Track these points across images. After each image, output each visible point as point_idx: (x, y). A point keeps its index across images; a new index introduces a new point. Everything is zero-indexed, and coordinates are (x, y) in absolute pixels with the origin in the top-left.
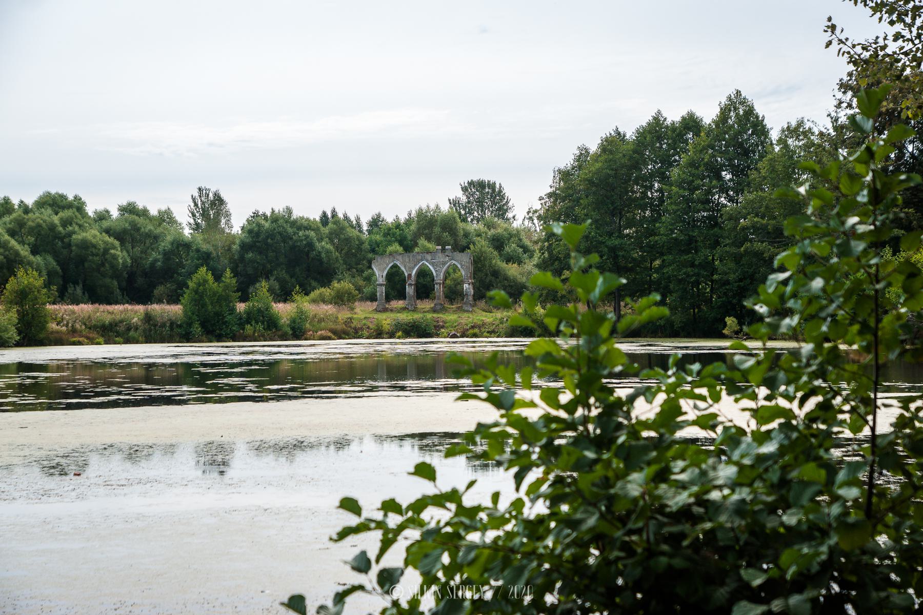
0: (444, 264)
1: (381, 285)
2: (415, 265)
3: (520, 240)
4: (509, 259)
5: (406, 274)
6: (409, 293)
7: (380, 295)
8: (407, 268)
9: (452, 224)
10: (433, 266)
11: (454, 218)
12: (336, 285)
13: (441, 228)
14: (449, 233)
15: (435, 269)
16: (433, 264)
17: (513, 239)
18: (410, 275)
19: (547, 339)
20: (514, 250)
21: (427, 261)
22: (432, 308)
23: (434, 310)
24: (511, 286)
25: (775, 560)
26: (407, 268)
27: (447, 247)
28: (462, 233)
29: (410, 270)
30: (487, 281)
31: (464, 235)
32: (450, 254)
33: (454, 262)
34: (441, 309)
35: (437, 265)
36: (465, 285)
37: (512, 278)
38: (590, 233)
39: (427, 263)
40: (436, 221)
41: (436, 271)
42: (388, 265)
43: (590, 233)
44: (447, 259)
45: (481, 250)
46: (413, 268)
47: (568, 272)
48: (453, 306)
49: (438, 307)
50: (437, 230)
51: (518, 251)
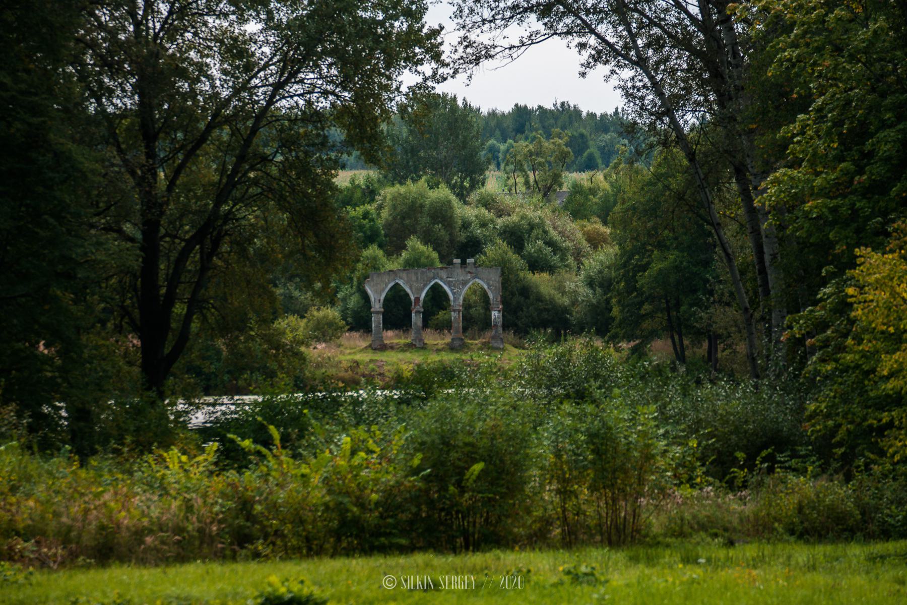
0: (465, 283)
1: (377, 313)
2: (425, 285)
3: (546, 232)
4: (535, 265)
5: (412, 298)
6: (416, 324)
7: (377, 326)
8: (414, 290)
9: (446, 211)
10: (449, 287)
11: (449, 202)
12: (315, 313)
13: (431, 217)
14: (443, 225)
15: (452, 290)
16: (449, 284)
17: (535, 232)
18: (417, 299)
19: (461, 324)
20: (540, 250)
21: (441, 279)
22: (448, 344)
23: (452, 348)
24: (548, 310)
25: (826, 427)
26: (414, 290)
27: (468, 261)
28: (460, 222)
29: (418, 293)
30: (514, 301)
31: (463, 226)
32: (474, 270)
33: (477, 280)
34: (460, 346)
35: (454, 286)
36: (493, 313)
37: (547, 297)
38: (681, 263)
39: (441, 283)
40: (422, 206)
41: (454, 294)
42: (386, 285)
43: (681, 263)
44: (469, 276)
45: (503, 258)
46: (422, 289)
47: (867, 499)
48: (476, 342)
49: (457, 343)
50: (424, 220)
51: (545, 252)
